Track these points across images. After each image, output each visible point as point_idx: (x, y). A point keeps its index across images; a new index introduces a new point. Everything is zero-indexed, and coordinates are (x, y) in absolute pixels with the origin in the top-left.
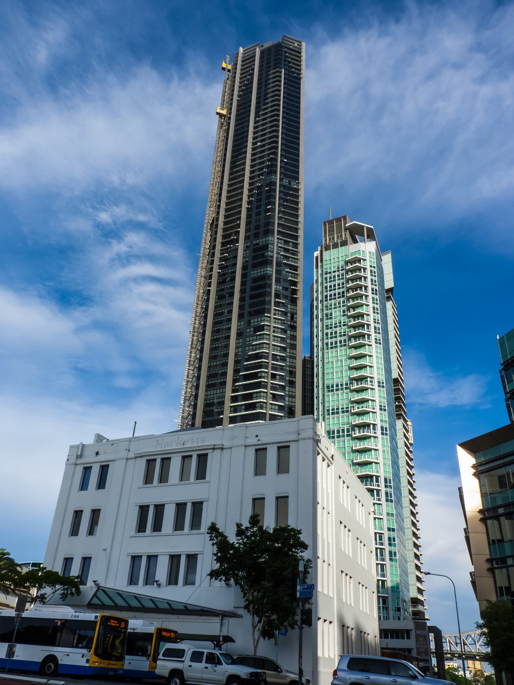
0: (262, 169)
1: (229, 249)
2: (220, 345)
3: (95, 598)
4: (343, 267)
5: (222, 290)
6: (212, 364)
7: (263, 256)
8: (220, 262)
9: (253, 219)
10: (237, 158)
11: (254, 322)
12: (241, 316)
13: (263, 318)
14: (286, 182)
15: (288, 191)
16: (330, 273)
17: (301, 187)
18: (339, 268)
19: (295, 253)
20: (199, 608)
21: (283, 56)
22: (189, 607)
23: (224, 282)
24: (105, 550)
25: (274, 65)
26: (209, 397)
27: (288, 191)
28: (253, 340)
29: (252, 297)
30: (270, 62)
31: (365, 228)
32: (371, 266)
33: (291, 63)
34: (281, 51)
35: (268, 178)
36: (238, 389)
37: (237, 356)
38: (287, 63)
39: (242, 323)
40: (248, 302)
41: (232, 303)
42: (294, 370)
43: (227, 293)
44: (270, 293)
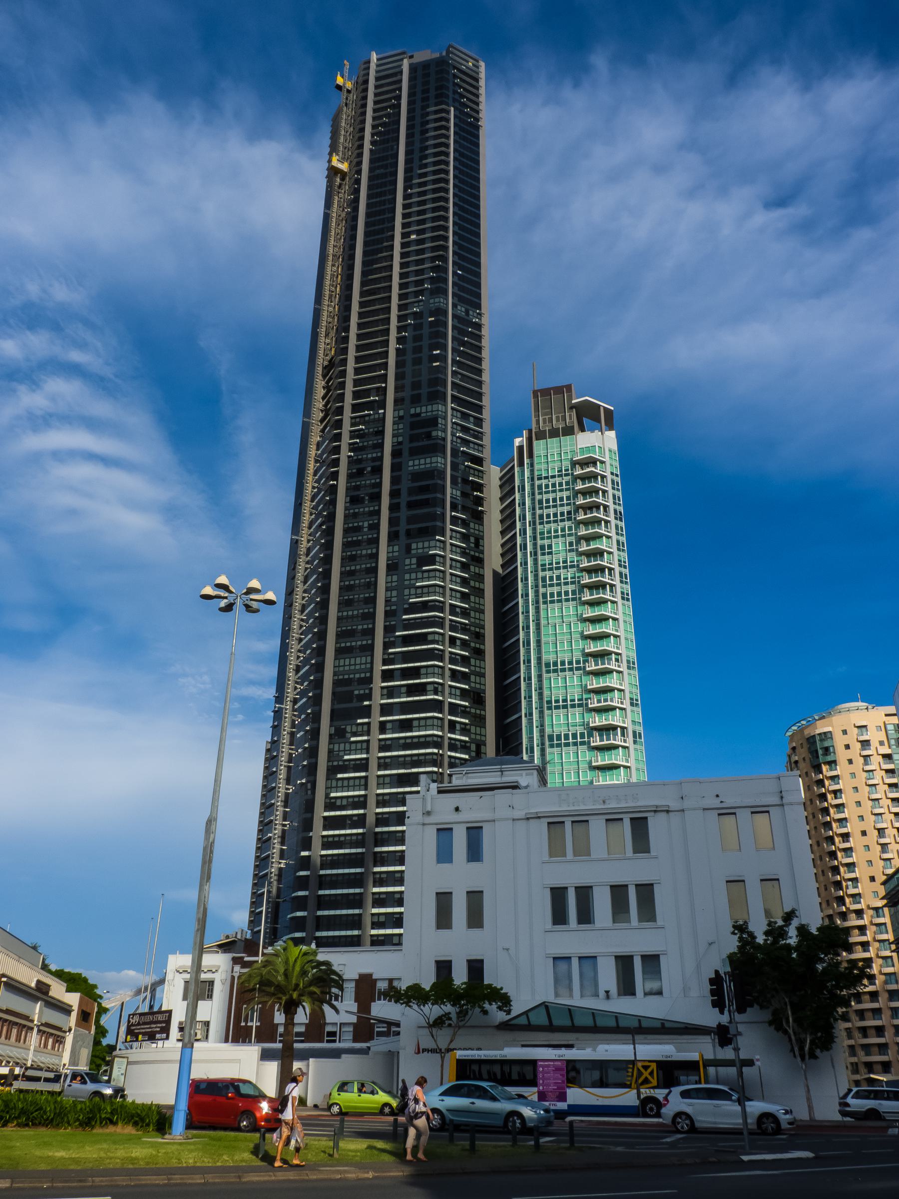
0: (421, 282)
1: (367, 418)
2: (357, 582)
3: (525, 1016)
4: (567, 470)
5: (357, 488)
6: (345, 614)
7: (429, 436)
8: (351, 438)
9: (408, 369)
10: (375, 257)
11: (417, 549)
12: (393, 537)
13: (432, 543)
14: (461, 309)
15: (465, 328)
16: (546, 478)
17: (485, 320)
18: (561, 471)
19: (479, 436)
20: (683, 1026)
21: (451, 84)
22: (667, 1025)
23: (360, 473)
24: (507, 950)
25: (437, 97)
26: (341, 669)
27: (465, 328)
28: (417, 579)
29: (411, 505)
30: (427, 91)
31: (602, 409)
32: (612, 473)
33: (464, 97)
34: (448, 73)
35: (432, 301)
36: (393, 659)
37: (389, 603)
38: (457, 97)
39: (396, 548)
40: (404, 513)
41: (378, 513)
42: (482, 631)
43: (367, 494)
44: (443, 501)
